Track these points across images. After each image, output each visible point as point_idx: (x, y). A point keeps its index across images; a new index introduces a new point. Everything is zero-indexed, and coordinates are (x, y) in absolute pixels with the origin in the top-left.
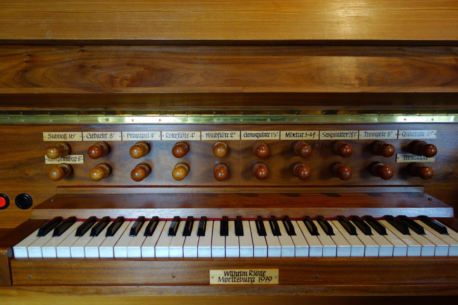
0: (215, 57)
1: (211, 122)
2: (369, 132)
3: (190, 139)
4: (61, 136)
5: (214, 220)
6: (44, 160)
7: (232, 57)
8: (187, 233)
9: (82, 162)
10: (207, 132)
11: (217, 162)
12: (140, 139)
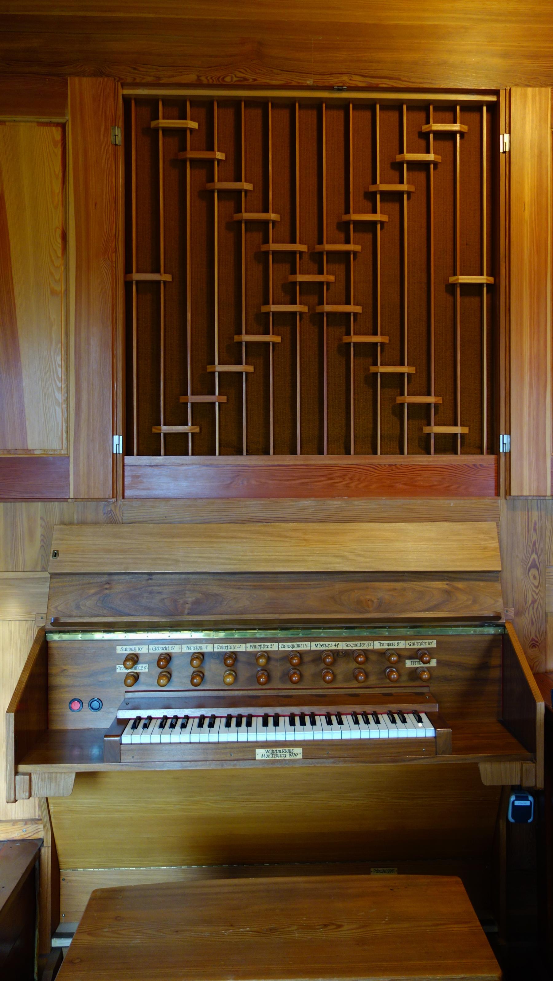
0: (258, 584)
1: (255, 636)
2: (382, 642)
3: (237, 650)
4: (131, 649)
5: (257, 716)
6: (115, 669)
7: (271, 583)
8: (239, 725)
9: (147, 670)
10: (251, 644)
11: (259, 669)
12: (196, 651)
